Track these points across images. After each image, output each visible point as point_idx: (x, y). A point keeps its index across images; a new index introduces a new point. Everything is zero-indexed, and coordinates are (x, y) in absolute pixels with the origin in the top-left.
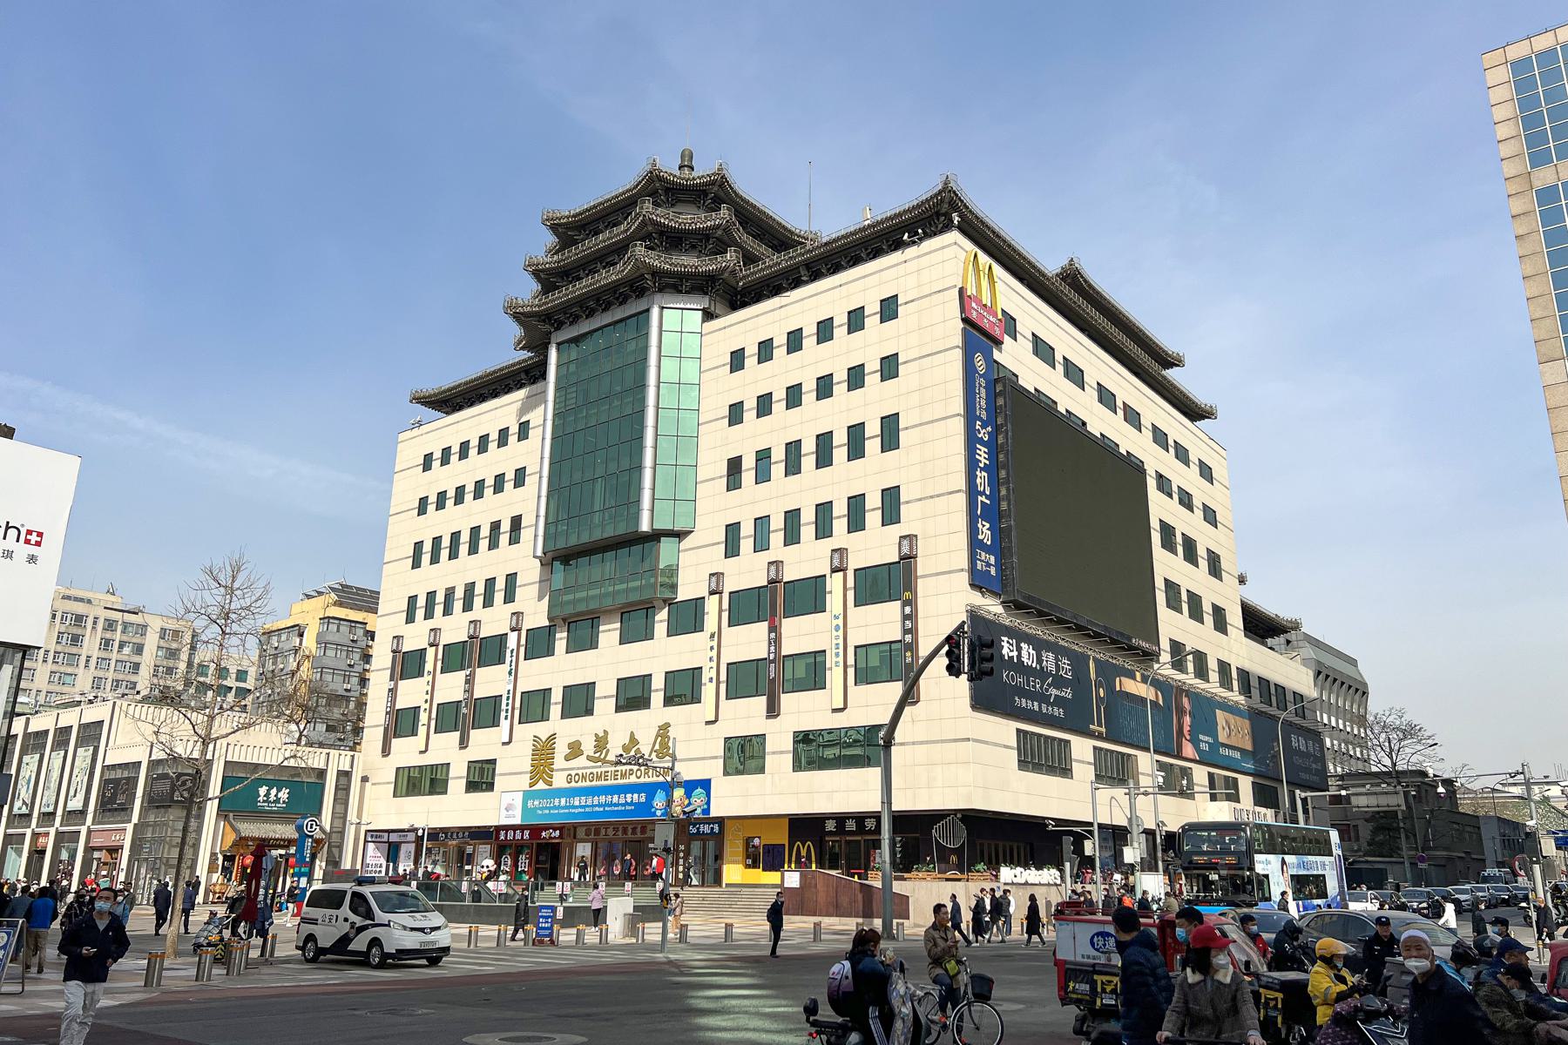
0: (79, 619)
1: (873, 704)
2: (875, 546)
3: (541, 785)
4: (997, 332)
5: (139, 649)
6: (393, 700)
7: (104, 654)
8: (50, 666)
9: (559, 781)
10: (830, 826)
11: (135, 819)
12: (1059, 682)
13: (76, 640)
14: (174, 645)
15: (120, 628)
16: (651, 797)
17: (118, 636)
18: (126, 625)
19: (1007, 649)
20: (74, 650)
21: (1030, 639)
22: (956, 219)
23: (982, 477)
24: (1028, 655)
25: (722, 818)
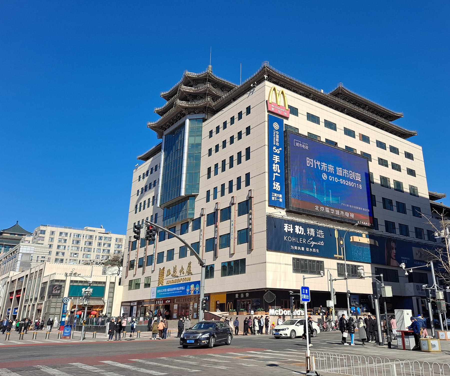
0: (91, 237)
1: (239, 251)
2: (240, 196)
3: (160, 285)
4: (285, 114)
5: (109, 245)
6: (129, 258)
7: (99, 248)
8: (83, 252)
9: (165, 284)
10: (237, 296)
11: (45, 300)
12: (316, 239)
13: (90, 243)
14: (120, 244)
15: (103, 239)
16: (186, 288)
17: (103, 241)
18: (106, 238)
19: (287, 228)
20: (90, 247)
21: (299, 224)
22: (266, 76)
23: (276, 167)
24: (299, 230)
25: (210, 294)
